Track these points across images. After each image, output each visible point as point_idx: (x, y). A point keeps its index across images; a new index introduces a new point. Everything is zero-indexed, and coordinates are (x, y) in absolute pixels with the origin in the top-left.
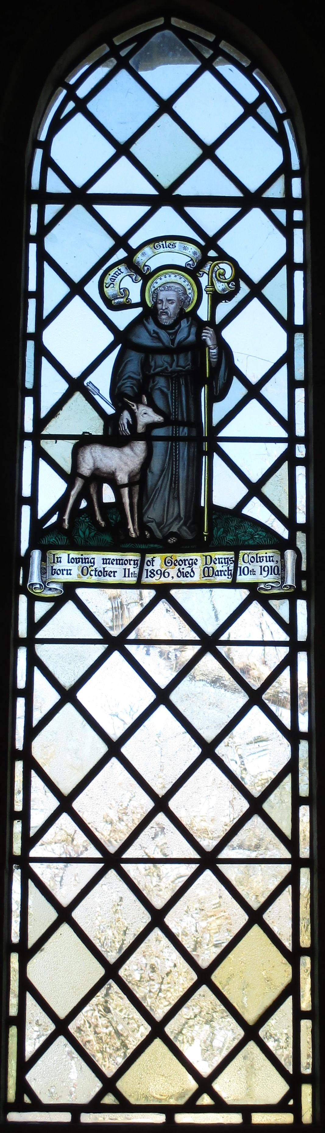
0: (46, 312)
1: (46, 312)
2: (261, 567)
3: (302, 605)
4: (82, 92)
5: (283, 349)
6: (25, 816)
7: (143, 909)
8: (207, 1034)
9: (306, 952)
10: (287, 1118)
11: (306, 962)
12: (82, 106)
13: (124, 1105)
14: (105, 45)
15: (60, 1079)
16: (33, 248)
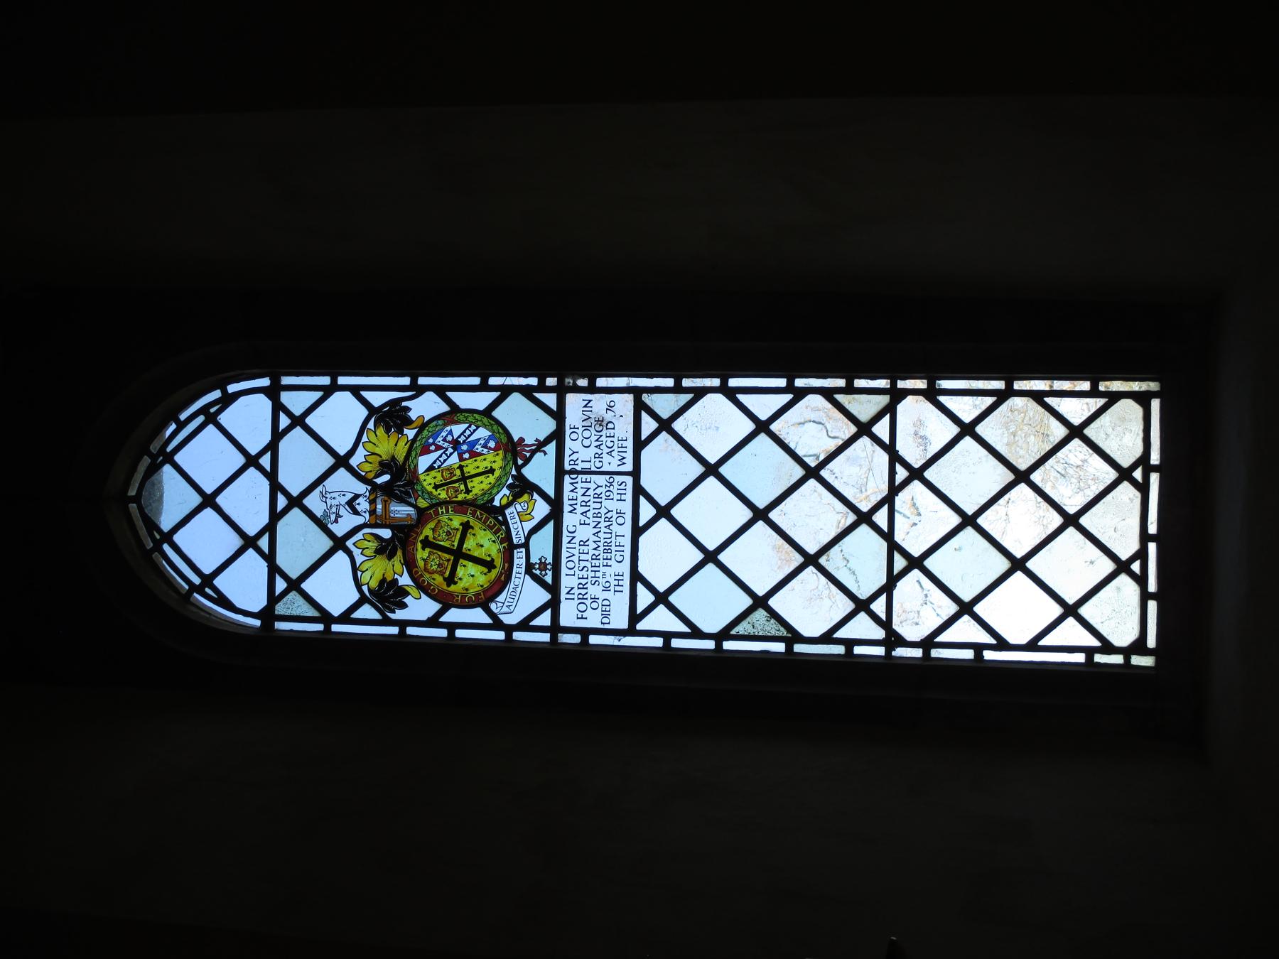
0: (685, 629)
1: (685, 629)
4: (196, 580)
5: (348, 394)
6: (978, 648)
7: (961, 533)
8: (1077, 474)
9: (414, 381)
10: (1155, 404)
11: (423, 381)
12: (208, 580)
13: (1142, 555)
16: (336, 628)
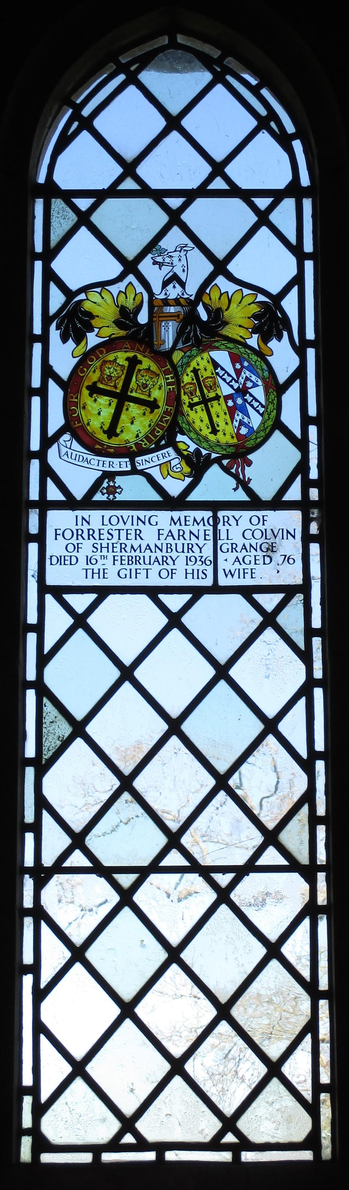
0: (47, 648)
1: (47, 648)
2: (187, 557)
3: (34, 495)
4: (86, 112)
10: (307, 1155)
12: (87, 124)
13: (142, 1145)
14: (112, 64)
15: (75, 1124)
16: (38, 265)
